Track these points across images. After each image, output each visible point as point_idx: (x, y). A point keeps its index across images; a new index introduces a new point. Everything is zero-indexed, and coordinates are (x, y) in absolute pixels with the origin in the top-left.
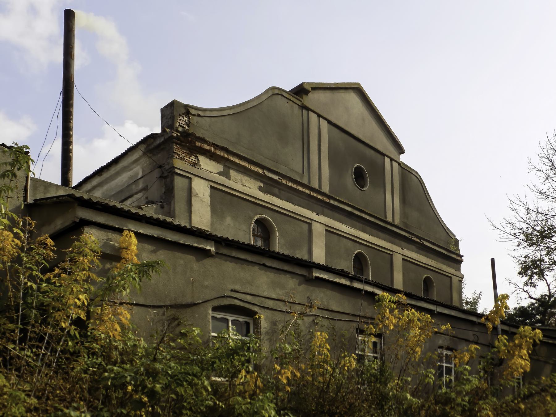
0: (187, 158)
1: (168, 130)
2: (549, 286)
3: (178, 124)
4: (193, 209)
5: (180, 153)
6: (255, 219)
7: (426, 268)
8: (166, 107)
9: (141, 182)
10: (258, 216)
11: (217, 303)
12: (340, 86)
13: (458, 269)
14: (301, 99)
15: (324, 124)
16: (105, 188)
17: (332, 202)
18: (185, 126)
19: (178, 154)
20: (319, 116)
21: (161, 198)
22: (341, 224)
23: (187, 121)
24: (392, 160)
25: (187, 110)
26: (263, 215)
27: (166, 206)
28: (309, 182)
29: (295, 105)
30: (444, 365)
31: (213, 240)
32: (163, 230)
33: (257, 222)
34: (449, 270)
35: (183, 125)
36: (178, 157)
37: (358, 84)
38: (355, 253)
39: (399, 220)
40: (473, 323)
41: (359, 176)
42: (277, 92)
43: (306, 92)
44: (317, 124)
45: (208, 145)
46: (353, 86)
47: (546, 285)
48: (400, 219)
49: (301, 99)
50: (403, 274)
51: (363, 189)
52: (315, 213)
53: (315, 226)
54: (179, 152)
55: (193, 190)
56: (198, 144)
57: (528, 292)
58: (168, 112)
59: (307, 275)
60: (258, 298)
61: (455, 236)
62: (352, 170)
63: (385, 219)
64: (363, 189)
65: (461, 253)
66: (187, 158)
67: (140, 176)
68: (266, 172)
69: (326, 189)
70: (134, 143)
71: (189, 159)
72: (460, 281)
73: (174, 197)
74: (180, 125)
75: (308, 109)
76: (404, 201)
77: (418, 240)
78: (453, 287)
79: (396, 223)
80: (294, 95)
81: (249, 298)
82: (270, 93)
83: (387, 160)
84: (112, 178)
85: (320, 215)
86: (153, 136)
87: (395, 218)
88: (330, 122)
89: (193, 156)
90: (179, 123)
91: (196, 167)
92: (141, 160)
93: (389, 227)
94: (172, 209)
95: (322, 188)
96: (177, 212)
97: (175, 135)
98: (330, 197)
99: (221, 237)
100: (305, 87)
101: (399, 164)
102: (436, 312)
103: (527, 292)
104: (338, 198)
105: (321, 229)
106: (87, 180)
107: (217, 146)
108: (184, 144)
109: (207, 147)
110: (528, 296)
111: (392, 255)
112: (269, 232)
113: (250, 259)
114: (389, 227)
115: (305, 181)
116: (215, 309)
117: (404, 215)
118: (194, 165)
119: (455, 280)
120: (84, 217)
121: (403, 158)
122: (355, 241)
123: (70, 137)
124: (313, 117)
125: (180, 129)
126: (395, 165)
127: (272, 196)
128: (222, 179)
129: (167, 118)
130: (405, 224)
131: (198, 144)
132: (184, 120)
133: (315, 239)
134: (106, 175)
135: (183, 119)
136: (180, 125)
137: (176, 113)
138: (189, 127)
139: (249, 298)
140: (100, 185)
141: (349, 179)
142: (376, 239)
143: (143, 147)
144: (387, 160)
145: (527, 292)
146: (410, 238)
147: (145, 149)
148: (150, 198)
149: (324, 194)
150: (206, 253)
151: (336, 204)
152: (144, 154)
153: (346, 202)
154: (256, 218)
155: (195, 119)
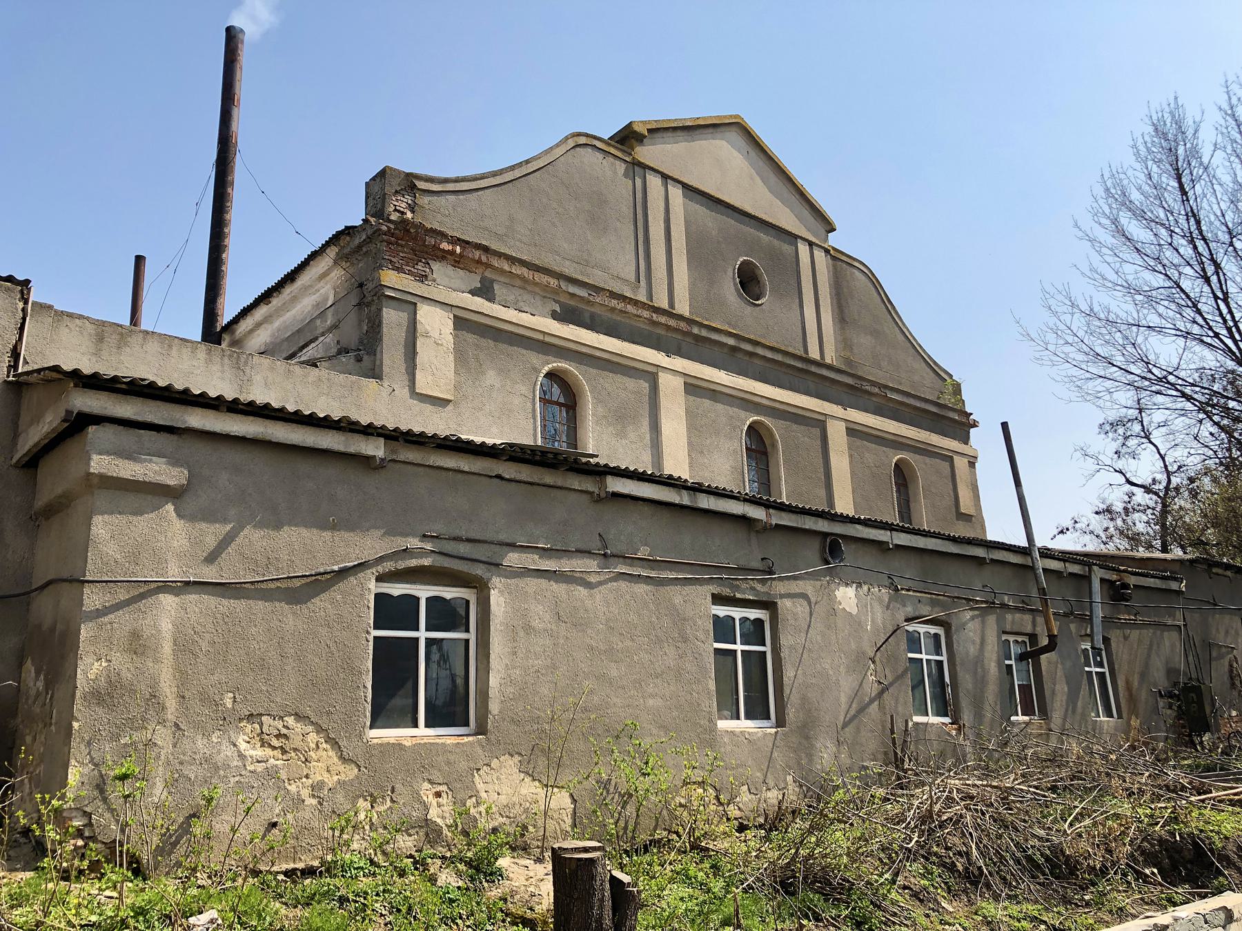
0: (409, 268)
1: (372, 220)
2: (1163, 458)
3: (392, 209)
4: (418, 360)
5: (393, 259)
6: (545, 372)
7: (897, 443)
8: (373, 179)
9: (330, 314)
10: (550, 366)
11: (389, 566)
12: (702, 122)
13: (966, 440)
14: (629, 151)
15: (676, 193)
16: (277, 324)
17: (696, 330)
18: (405, 211)
19: (391, 261)
20: (665, 177)
21: (361, 342)
22: (715, 371)
23: (410, 202)
24: (811, 244)
25: (410, 183)
26: (560, 364)
27: (365, 358)
28: (650, 297)
29: (618, 162)
30: (924, 656)
31: (379, 435)
32: (267, 422)
33: (551, 375)
34: (949, 444)
35: (402, 209)
36: (391, 267)
37: (737, 116)
38: (748, 423)
39: (833, 354)
40: (980, 561)
41: (749, 282)
42: (583, 140)
43: (640, 138)
44: (663, 192)
45: (448, 243)
46: (727, 121)
47: (1158, 456)
48: (836, 351)
49: (629, 151)
50: (851, 456)
51: (757, 302)
52: (664, 354)
53: (663, 378)
54: (394, 257)
55: (419, 326)
56: (430, 241)
57: (1124, 471)
58: (376, 188)
59: (597, 491)
60: (486, 546)
61: (951, 376)
62: (734, 269)
63: (804, 356)
64: (757, 302)
65: (968, 410)
66: (409, 268)
67: (330, 303)
68: (563, 285)
69: (683, 308)
70: (318, 245)
71: (412, 269)
72: (972, 465)
73: (381, 340)
74: (395, 210)
75: (645, 167)
76: (842, 319)
77: (877, 390)
78: (957, 477)
79: (828, 361)
80: (619, 146)
81: (463, 549)
82: (571, 143)
83: (803, 249)
84: (284, 308)
85: (673, 356)
86: (349, 231)
87: (826, 351)
88: (686, 187)
89: (420, 264)
90: (395, 206)
91: (426, 282)
92: (333, 274)
93: (813, 369)
94: (378, 363)
95: (676, 307)
96: (386, 369)
97: (384, 228)
98: (690, 322)
99: (396, 430)
100: (636, 128)
101: (827, 251)
102: (891, 546)
103: (1121, 472)
104: (706, 323)
105: (679, 382)
106: (245, 312)
107: (468, 243)
108: (404, 243)
109: (445, 246)
110: (1124, 480)
111: (825, 422)
112: (574, 395)
113: (466, 469)
114: (813, 369)
115: (642, 297)
116: (380, 579)
117: (845, 343)
118: (422, 278)
119: (961, 464)
120: (86, 409)
121: (834, 240)
122: (747, 402)
123: (225, 238)
124: (654, 182)
125: (394, 216)
126: (819, 255)
127: (577, 328)
128: (478, 303)
129: (374, 199)
130: (848, 362)
131: (430, 241)
132: (406, 200)
133: (664, 402)
134: (276, 302)
135: (402, 199)
136: (395, 210)
137: (388, 189)
138: (413, 212)
139: (463, 549)
140: (266, 320)
141: (729, 288)
142: (790, 393)
143: (332, 252)
144: (803, 249)
145: (1121, 472)
146: (859, 386)
147: (337, 254)
148: (344, 343)
149: (680, 317)
150: (365, 461)
151: (704, 333)
152: (336, 262)
153: (725, 327)
154: (546, 369)
155: (424, 200)
